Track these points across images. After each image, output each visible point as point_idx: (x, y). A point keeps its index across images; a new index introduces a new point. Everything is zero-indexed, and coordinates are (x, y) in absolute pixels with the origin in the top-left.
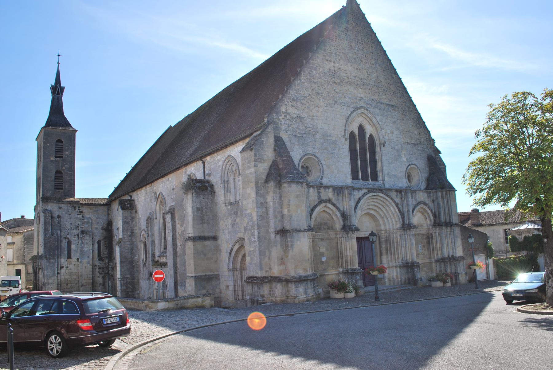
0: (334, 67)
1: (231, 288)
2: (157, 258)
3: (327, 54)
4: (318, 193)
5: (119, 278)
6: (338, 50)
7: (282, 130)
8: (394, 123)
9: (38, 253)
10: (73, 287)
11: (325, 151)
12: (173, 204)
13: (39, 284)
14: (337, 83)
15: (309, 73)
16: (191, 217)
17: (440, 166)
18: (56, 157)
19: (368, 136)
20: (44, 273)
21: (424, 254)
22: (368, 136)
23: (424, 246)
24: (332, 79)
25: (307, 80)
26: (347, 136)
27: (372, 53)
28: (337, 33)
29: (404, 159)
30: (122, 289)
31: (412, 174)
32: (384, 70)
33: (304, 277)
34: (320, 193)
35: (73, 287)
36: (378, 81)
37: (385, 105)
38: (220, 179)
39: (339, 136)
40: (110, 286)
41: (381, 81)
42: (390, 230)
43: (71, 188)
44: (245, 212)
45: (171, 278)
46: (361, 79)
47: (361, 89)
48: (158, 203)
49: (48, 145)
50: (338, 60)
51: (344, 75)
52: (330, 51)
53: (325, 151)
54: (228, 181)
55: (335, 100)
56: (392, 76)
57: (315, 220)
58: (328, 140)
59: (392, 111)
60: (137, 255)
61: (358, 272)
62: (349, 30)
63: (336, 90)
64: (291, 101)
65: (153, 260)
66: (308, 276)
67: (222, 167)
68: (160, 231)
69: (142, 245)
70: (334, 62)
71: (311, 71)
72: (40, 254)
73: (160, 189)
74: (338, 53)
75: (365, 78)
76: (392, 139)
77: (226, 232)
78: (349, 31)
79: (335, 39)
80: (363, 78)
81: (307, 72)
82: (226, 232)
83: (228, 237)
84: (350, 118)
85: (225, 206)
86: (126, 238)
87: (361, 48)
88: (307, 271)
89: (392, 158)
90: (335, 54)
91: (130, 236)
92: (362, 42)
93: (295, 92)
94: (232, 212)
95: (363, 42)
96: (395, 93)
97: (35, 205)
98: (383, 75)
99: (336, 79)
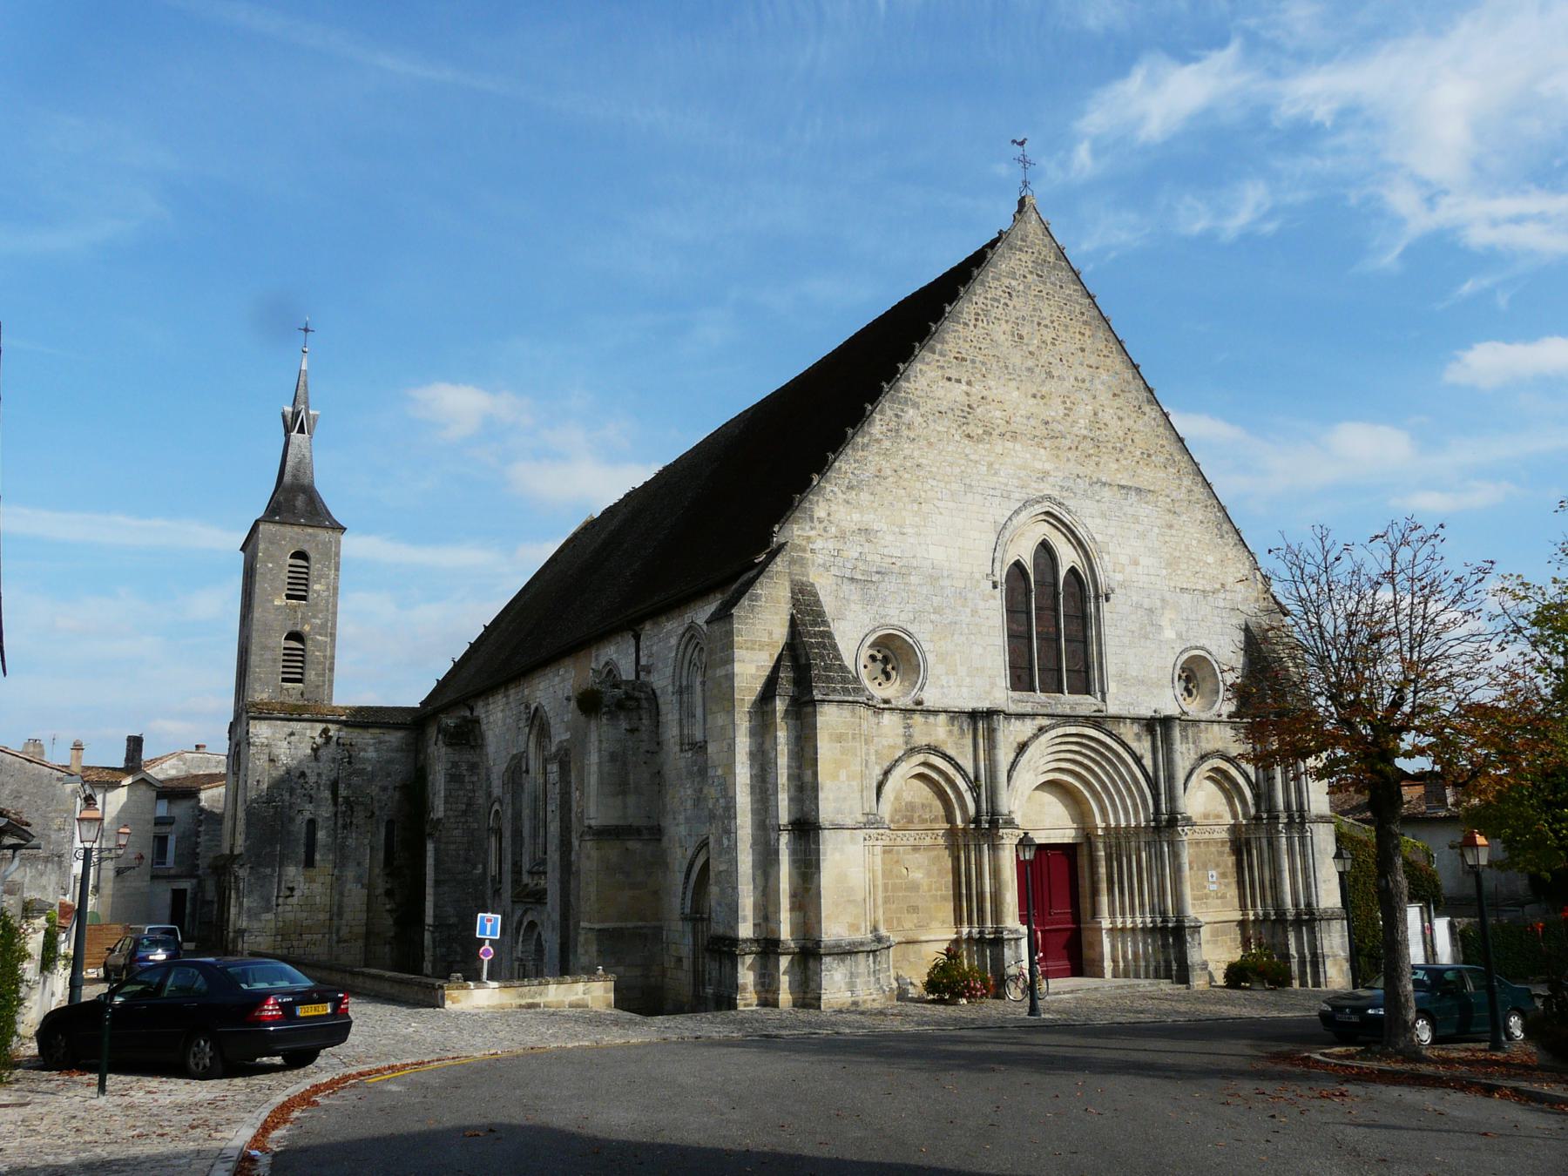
0: (968, 394)
1: (687, 964)
2: (526, 879)
3: (950, 362)
4: (905, 728)
5: (429, 926)
6: (980, 349)
8: (1143, 536)
9: (232, 851)
10: (315, 944)
11: (933, 617)
12: (567, 736)
13: (228, 932)
15: (897, 415)
16: (596, 776)
18: (289, 597)
19: (1062, 573)
20: (241, 904)
21: (1223, 897)
22: (1062, 573)
23: (1224, 875)
24: (959, 426)
25: (889, 434)
26: (1001, 574)
27: (1083, 350)
28: (980, 305)
29: (1169, 634)
30: (434, 955)
32: (1115, 395)
33: (849, 944)
35: (315, 944)
36: (1097, 425)
37: (1116, 488)
38: (670, 680)
39: (978, 576)
40: (1267, 883)
41: (1105, 424)
42: (1118, 827)
43: (324, 681)
44: (711, 773)
45: (553, 930)
46: (1047, 423)
47: (1045, 448)
48: (534, 732)
49: (270, 565)
50: (979, 375)
51: (998, 414)
52: (959, 352)
53: (933, 617)
54: (690, 687)
55: (968, 481)
56: (1140, 408)
57: (897, 798)
58: (942, 588)
59: (1135, 504)
60: (480, 866)
61: (1011, 940)
62: (1014, 294)
63: (972, 457)
64: (844, 489)
65: (517, 881)
66: (862, 944)
67: (677, 652)
68: (535, 806)
69: (493, 839)
70: (969, 383)
71: (902, 411)
72: (236, 852)
73: (539, 694)
74: (980, 358)
75: (1058, 418)
77: (681, 818)
78: (1015, 298)
79: (973, 322)
80: (1050, 419)
81: (889, 413)
82: (681, 818)
83: (682, 830)
84: (1010, 528)
85: (681, 751)
86: (452, 820)
87: (1049, 341)
88: (858, 929)
89: (1133, 632)
90: (973, 362)
91: (465, 813)
92: (1052, 322)
93: (857, 465)
94: (695, 768)
95: (1055, 324)
96: (1149, 456)
97: (231, 719)
98: (1112, 408)
99: (972, 427)
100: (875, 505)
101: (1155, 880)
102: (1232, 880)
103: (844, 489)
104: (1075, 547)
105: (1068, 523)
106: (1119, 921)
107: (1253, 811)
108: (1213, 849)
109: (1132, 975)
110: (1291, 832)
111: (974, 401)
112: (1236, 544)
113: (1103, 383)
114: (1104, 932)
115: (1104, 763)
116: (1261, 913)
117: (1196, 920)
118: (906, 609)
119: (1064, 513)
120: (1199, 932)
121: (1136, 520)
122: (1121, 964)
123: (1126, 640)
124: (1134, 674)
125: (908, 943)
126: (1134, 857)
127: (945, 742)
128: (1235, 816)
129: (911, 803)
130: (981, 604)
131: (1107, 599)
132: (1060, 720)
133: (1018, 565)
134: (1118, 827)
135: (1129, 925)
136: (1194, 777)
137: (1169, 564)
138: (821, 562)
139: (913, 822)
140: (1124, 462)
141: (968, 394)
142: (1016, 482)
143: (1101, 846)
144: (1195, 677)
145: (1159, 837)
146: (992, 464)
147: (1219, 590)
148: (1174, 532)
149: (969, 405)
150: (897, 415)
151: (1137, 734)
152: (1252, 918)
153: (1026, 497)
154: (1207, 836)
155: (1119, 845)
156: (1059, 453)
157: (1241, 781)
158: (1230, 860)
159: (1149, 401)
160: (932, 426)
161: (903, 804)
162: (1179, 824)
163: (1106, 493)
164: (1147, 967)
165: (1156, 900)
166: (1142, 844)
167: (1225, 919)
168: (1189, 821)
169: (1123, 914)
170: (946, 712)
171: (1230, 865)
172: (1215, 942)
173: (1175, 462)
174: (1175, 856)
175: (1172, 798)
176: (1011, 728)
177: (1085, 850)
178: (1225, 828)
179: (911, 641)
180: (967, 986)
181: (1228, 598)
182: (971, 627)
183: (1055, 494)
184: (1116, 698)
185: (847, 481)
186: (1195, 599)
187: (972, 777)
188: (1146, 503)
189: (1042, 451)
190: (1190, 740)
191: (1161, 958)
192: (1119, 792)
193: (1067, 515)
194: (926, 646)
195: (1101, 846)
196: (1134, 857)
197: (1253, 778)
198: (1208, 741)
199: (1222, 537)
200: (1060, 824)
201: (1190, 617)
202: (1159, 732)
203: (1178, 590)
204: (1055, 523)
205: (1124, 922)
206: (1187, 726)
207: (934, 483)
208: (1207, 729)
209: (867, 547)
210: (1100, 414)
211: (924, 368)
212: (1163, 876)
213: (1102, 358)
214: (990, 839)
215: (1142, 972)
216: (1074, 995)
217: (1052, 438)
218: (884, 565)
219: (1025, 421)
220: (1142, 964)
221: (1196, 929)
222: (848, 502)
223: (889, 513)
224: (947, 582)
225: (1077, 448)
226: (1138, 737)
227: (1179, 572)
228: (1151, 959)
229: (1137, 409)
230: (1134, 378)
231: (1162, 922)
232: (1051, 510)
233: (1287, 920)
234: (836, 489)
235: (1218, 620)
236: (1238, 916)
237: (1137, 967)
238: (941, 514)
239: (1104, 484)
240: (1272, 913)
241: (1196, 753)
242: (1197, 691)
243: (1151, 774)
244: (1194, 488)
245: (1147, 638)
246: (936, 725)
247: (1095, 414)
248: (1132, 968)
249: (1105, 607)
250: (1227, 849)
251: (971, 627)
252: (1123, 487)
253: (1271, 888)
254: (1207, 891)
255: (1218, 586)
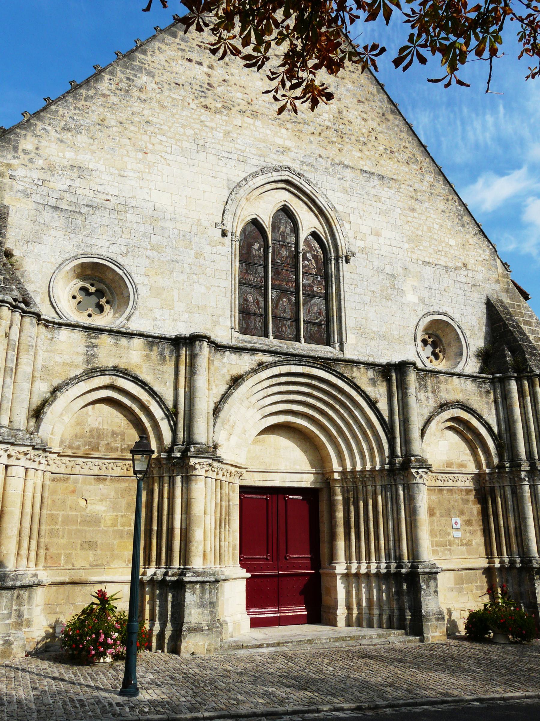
4: (88, 347)
7: (15, 190)
11: (149, 253)
14: (213, 109)
15: (128, 79)
17: (507, 322)
21: (468, 544)
23: (469, 523)
25: (117, 92)
29: (411, 298)
31: (443, 340)
32: (359, 101)
34: (96, 346)
36: (341, 121)
40: (512, 531)
42: (353, 471)
47: (287, 129)
51: (239, 95)
53: (149, 253)
55: (201, 142)
58: (163, 228)
61: (196, 583)
64: (58, 129)
76: (375, 247)
81: (120, 75)
93: (77, 112)
100: (94, 148)
101: (390, 523)
102: (478, 528)
103: (58, 129)
104: (316, 216)
105: (309, 192)
106: (374, 566)
107: (496, 461)
108: (457, 497)
109: (364, 624)
110: (534, 481)
111: (214, 81)
112: (476, 234)
113: (348, 91)
114: (338, 577)
115: (337, 407)
116: (507, 560)
117: (434, 566)
118: (119, 242)
119: (304, 183)
120: (435, 579)
121: (379, 199)
122: (355, 612)
123: (367, 299)
124: (375, 329)
125: (74, 583)
126: (370, 502)
127: (139, 367)
128: (479, 465)
129: (98, 429)
130: (207, 249)
131: (347, 261)
132: (284, 358)
133: (255, 222)
134: (353, 471)
135: (363, 571)
136: (433, 424)
137: (410, 240)
138: (21, 188)
139: (98, 450)
140: (367, 153)
141: (208, 75)
142: (254, 151)
143: (338, 490)
144: (442, 342)
145: (395, 480)
146: (229, 133)
147: (460, 268)
148: (416, 215)
149: (208, 84)
150: (128, 79)
151: (371, 379)
152: (497, 565)
153: (264, 164)
154: (450, 484)
155: (356, 490)
156: (301, 135)
157: (483, 431)
158: (476, 508)
159: (392, 112)
160: (167, 93)
161: (88, 429)
162: (412, 465)
163: (348, 173)
164: (380, 615)
165: (391, 544)
166: (379, 488)
167: (470, 566)
168: (424, 464)
169: (359, 559)
170: (142, 335)
171: (475, 512)
172: (460, 590)
173: (417, 161)
174: (410, 499)
175: (407, 441)
176: (225, 360)
177: (324, 496)
178: (470, 477)
179: (121, 272)
180: (96, 642)
181: (470, 275)
182: (194, 267)
183: (296, 166)
184: (354, 349)
185: (64, 123)
186: (437, 272)
187: (170, 405)
188: (388, 187)
189: (283, 131)
190: (429, 388)
191: (395, 606)
192: (355, 436)
193: (307, 185)
194: (137, 279)
195: (338, 490)
196: (370, 502)
197: (496, 430)
198: (448, 391)
199: (463, 226)
200: (298, 468)
201: (433, 286)
202: (394, 377)
203: (420, 262)
204: (296, 192)
205: (359, 568)
206: (425, 376)
207: (164, 139)
208: (446, 380)
209: (78, 182)
210: (345, 113)
211: (163, 47)
212: (399, 519)
213: (348, 73)
214: (184, 469)
215: (375, 619)
216: (279, 649)
217: (295, 122)
218: (97, 200)
219: (267, 105)
220: (376, 612)
221: (432, 575)
222: (62, 141)
223: (108, 156)
224: (168, 224)
225: (320, 134)
226: (373, 382)
227: (421, 248)
228: (385, 607)
229: (381, 115)
230: (378, 92)
231: (396, 568)
232: (290, 179)
233: (533, 568)
234: (49, 128)
235: (460, 292)
236: (484, 563)
237: (371, 615)
238: (169, 165)
239: (347, 167)
240: (518, 560)
241: (435, 402)
242: (444, 354)
243: (387, 419)
244: (436, 184)
245: (388, 299)
246: (129, 348)
247: (339, 112)
248: (365, 617)
249: (344, 267)
250: (472, 497)
251: (194, 267)
252: (366, 172)
253: (516, 535)
254: (450, 538)
255: (460, 265)
